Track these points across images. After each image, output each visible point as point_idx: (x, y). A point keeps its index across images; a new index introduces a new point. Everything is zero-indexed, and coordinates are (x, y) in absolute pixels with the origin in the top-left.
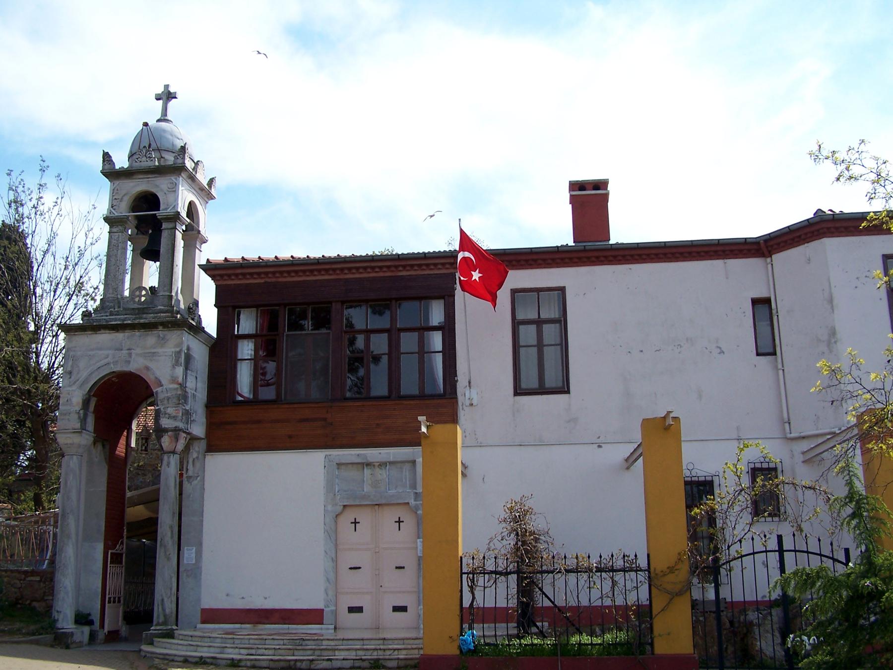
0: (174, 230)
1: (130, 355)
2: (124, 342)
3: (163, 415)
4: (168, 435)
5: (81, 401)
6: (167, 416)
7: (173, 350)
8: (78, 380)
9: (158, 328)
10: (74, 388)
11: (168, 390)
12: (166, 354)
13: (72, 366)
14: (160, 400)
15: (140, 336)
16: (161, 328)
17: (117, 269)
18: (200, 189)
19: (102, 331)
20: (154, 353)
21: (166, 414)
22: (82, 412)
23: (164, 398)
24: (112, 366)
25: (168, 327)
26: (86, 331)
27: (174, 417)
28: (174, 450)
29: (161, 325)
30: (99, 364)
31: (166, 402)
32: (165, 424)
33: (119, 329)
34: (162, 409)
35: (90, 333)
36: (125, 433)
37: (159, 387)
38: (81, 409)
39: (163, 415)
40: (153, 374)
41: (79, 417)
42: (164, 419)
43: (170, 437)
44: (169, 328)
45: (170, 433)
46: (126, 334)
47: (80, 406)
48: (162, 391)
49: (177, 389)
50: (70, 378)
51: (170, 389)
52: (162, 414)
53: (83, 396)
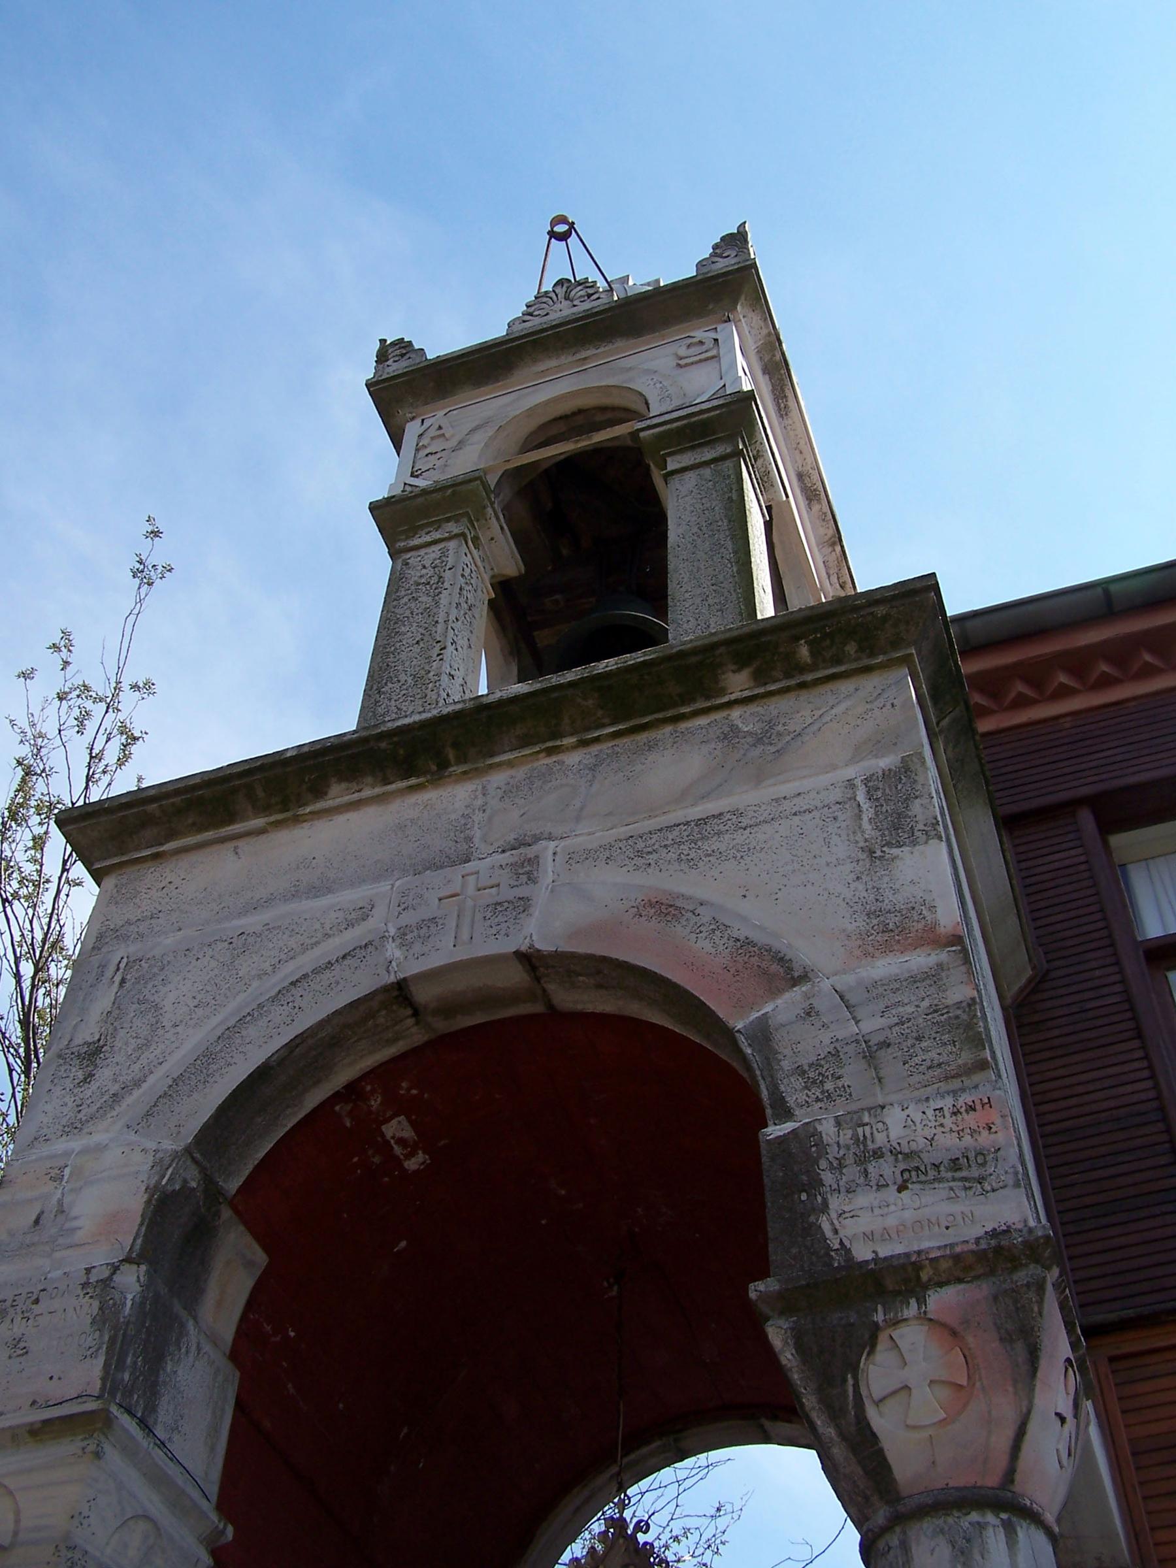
0: (729, 463)
1: (527, 870)
2: (478, 817)
3: (852, 1172)
4: (924, 1318)
5: (135, 1203)
6: (887, 1168)
7: (850, 772)
8: (138, 1083)
9: (722, 691)
10: (100, 1134)
11: (852, 998)
12: (802, 803)
13: (113, 1016)
14: (801, 1071)
15: (593, 768)
16: (738, 682)
17: (436, 650)
18: (800, 476)
19: (338, 793)
20: (702, 821)
21: (867, 1155)
22: (131, 1280)
23: (835, 1054)
24: (393, 951)
25: (794, 668)
26: (231, 818)
27: (955, 1164)
28: (1010, 1475)
29: (741, 661)
30: (291, 970)
31: (853, 1073)
32: (869, 1237)
33: (451, 754)
34: (827, 1129)
35: (259, 822)
36: (753, 403)
37: (774, 992)
38: (128, 1260)
39: (852, 1172)
40: (719, 926)
41: (105, 1317)
42: (863, 1199)
43: (949, 1332)
44: (802, 669)
45: (941, 1300)
46: (498, 779)
47: (128, 1235)
48: (809, 1012)
49: (934, 976)
50: (88, 1078)
51: (872, 988)
52: (839, 1166)
53: (159, 1165)
